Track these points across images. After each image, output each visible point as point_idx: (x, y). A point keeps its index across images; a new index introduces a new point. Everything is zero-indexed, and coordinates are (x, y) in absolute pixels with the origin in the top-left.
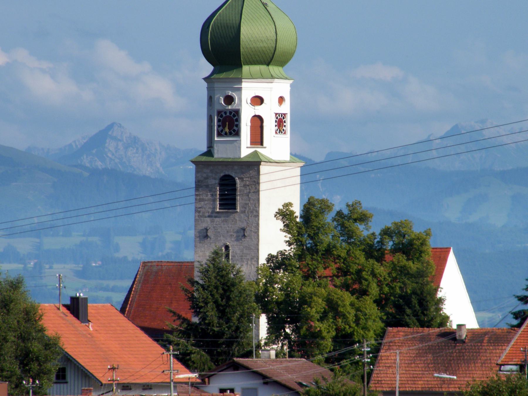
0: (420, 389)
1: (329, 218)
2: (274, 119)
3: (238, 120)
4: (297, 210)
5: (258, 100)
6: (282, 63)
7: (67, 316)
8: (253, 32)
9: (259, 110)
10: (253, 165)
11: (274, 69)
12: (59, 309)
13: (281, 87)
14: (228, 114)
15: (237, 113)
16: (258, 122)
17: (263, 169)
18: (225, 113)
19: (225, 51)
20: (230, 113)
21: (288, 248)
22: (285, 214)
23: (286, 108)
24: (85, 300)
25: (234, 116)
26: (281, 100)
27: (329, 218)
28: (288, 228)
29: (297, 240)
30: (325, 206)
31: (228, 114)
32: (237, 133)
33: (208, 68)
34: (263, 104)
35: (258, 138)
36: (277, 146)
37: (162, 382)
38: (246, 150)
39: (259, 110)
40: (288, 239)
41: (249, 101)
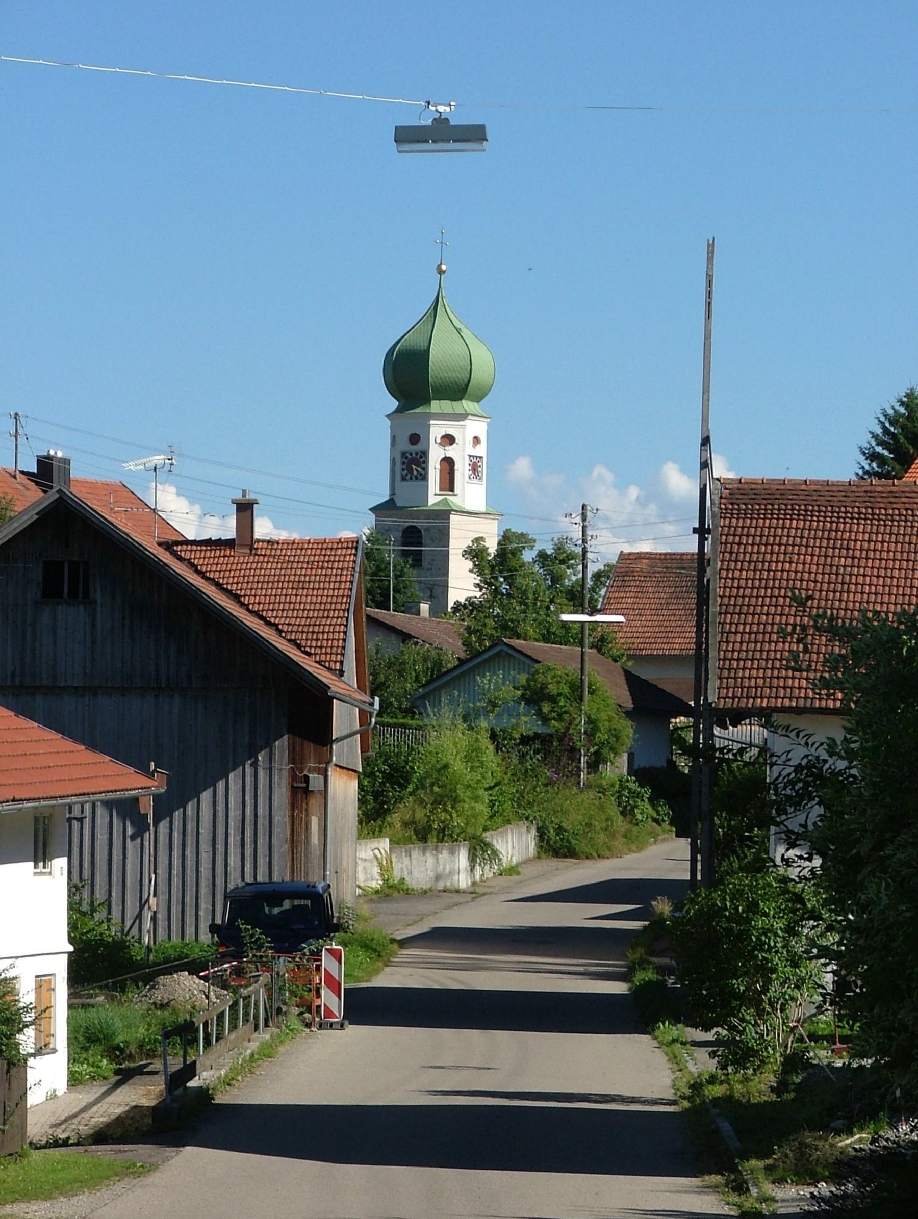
0: (677, 652)
1: (528, 556)
2: (467, 462)
3: (426, 462)
4: (492, 546)
5: (449, 440)
6: (478, 398)
7: (28, 489)
8: (443, 354)
9: (451, 451)
10: (443, 514)
11: (467, 405)
12: (15, 477)
13: (476, 427)
14: (414, 455)
15: (425, 454)
16: (448, 463)
17: (453, 518)
18: (411, 454)
19: (412, 379)
20: (417, 454)
21: (478, 594)
22: (475, 553)
23: (481, 450)
24: (66, 461)
25: (421, 457)
26: (476, 440)
27: (528, 556)
28: (479, 569)
29: (487, 583)
30: (524, 540)
31: (414, 455)
32: (424, 477)
33: (394, 404)
34: (455, 445)
35: (448, 484)
36: (471, 494)
37: (125, 534)
38: (433, 499)
39: (451, 451)
40: (477, 582)
41: (438, 441)
